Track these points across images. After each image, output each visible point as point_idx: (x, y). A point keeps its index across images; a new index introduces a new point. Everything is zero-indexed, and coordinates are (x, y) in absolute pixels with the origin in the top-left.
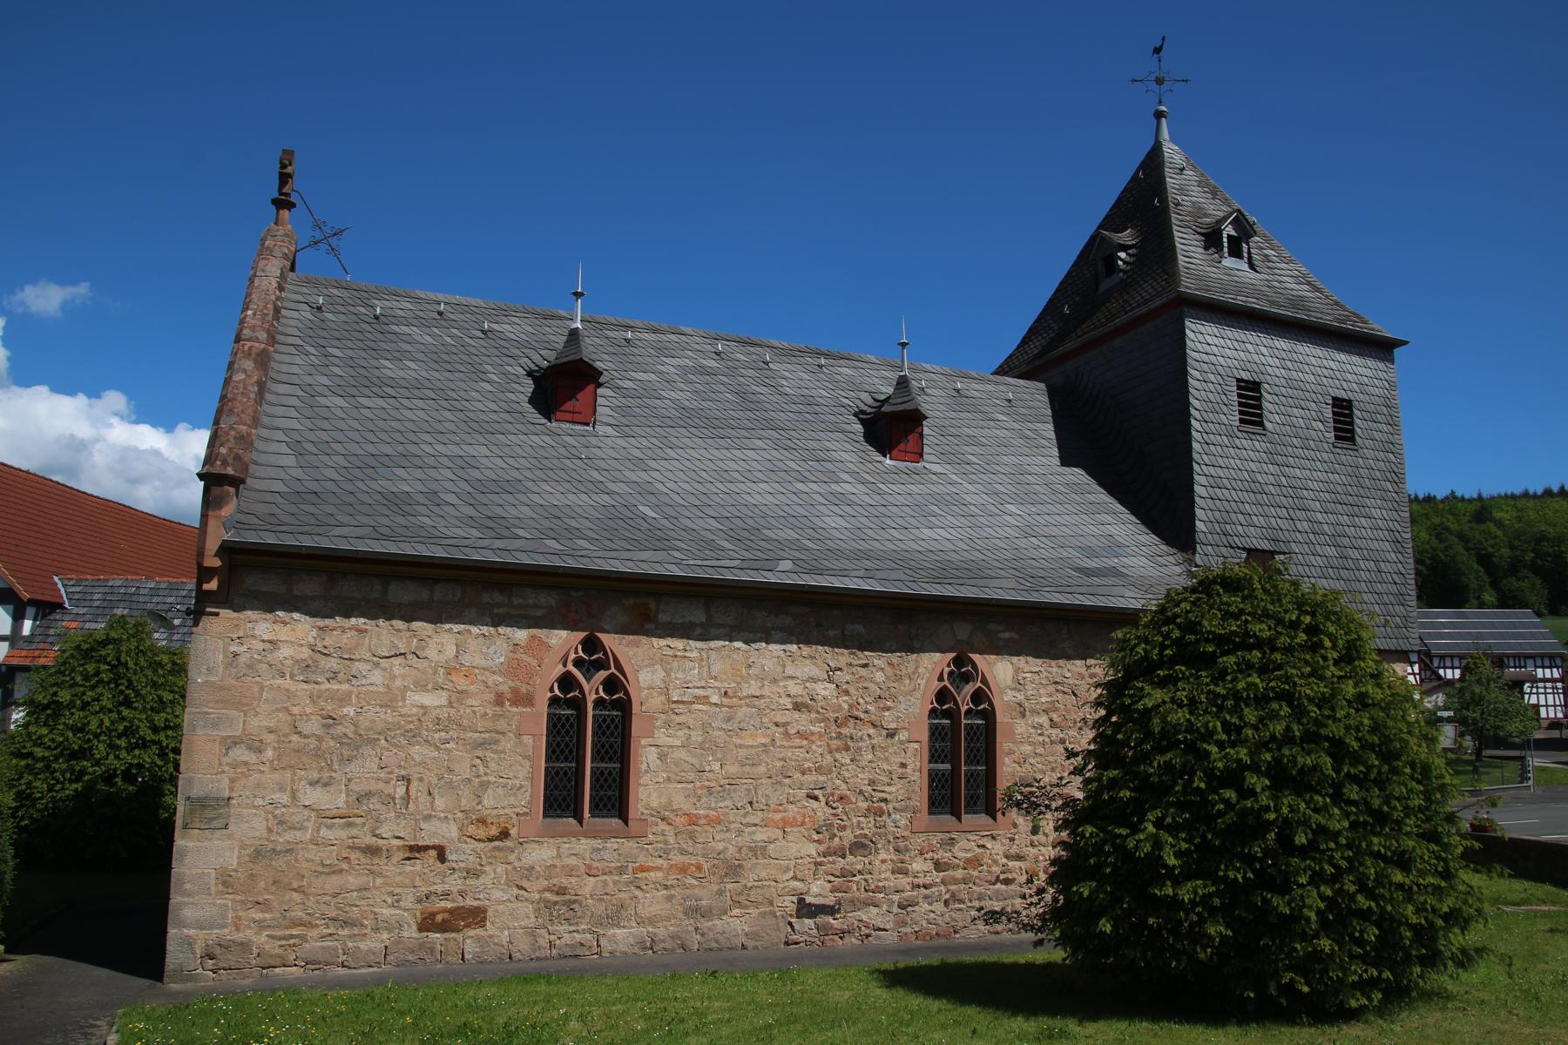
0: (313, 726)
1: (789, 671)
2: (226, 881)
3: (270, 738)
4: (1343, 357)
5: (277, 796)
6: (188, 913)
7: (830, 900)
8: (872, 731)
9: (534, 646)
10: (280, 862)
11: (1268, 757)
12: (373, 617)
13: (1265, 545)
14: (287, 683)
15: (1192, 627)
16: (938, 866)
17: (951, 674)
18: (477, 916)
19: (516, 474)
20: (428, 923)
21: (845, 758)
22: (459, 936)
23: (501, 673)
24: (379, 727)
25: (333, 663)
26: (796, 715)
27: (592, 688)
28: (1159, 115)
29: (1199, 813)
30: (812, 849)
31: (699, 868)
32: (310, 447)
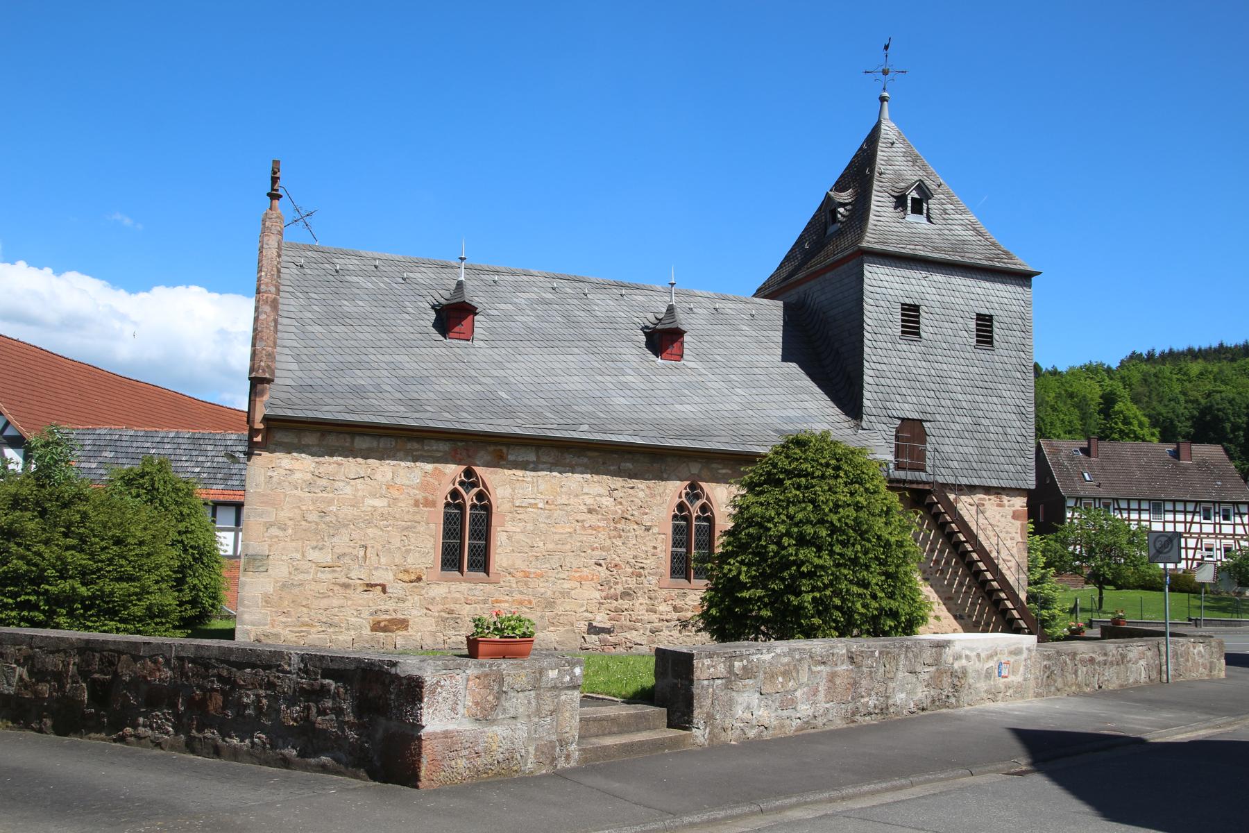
0: (314, 517)
1: (585, 490)
2: (267, 601)
3: (290, 523)
4: (988, 285)
5: (294, 555)
6: (246, 617)
7: (608, 625)
8: (636, 527)
9: (437, 474)
10: (296, 591)
11: (796, 530)
12: (346, 457)
13: (916, 416)
14: (299, 493)
15: (775, 465)
16: (675, 609)
17: (687, 494)
18: (403, 624)
19: (425, 373)
20: (376, 627)
21: (619, 542)
22: (393, 635)
23: (417, 488)
24: (350, 517)
25: (324, 482)
26: (589, 516)
27: (469, 498)
28: (883, 99)
29: (762, 555)
30: (597, 595)
31: (530, 602)
32: (305, 357)
